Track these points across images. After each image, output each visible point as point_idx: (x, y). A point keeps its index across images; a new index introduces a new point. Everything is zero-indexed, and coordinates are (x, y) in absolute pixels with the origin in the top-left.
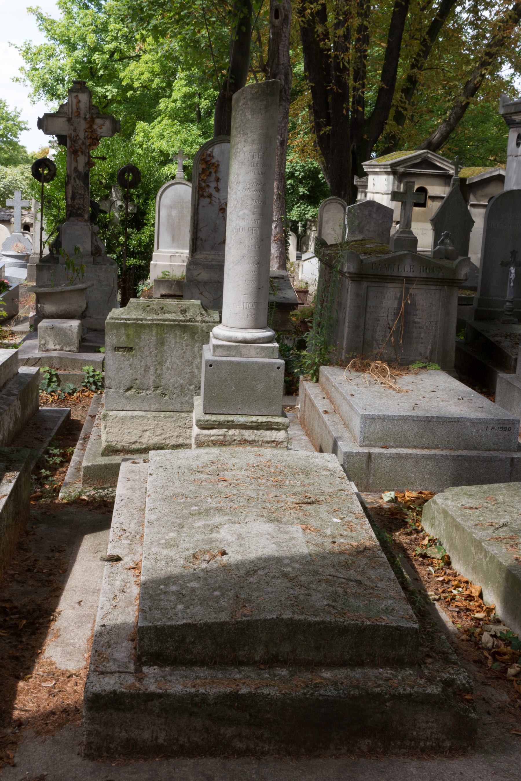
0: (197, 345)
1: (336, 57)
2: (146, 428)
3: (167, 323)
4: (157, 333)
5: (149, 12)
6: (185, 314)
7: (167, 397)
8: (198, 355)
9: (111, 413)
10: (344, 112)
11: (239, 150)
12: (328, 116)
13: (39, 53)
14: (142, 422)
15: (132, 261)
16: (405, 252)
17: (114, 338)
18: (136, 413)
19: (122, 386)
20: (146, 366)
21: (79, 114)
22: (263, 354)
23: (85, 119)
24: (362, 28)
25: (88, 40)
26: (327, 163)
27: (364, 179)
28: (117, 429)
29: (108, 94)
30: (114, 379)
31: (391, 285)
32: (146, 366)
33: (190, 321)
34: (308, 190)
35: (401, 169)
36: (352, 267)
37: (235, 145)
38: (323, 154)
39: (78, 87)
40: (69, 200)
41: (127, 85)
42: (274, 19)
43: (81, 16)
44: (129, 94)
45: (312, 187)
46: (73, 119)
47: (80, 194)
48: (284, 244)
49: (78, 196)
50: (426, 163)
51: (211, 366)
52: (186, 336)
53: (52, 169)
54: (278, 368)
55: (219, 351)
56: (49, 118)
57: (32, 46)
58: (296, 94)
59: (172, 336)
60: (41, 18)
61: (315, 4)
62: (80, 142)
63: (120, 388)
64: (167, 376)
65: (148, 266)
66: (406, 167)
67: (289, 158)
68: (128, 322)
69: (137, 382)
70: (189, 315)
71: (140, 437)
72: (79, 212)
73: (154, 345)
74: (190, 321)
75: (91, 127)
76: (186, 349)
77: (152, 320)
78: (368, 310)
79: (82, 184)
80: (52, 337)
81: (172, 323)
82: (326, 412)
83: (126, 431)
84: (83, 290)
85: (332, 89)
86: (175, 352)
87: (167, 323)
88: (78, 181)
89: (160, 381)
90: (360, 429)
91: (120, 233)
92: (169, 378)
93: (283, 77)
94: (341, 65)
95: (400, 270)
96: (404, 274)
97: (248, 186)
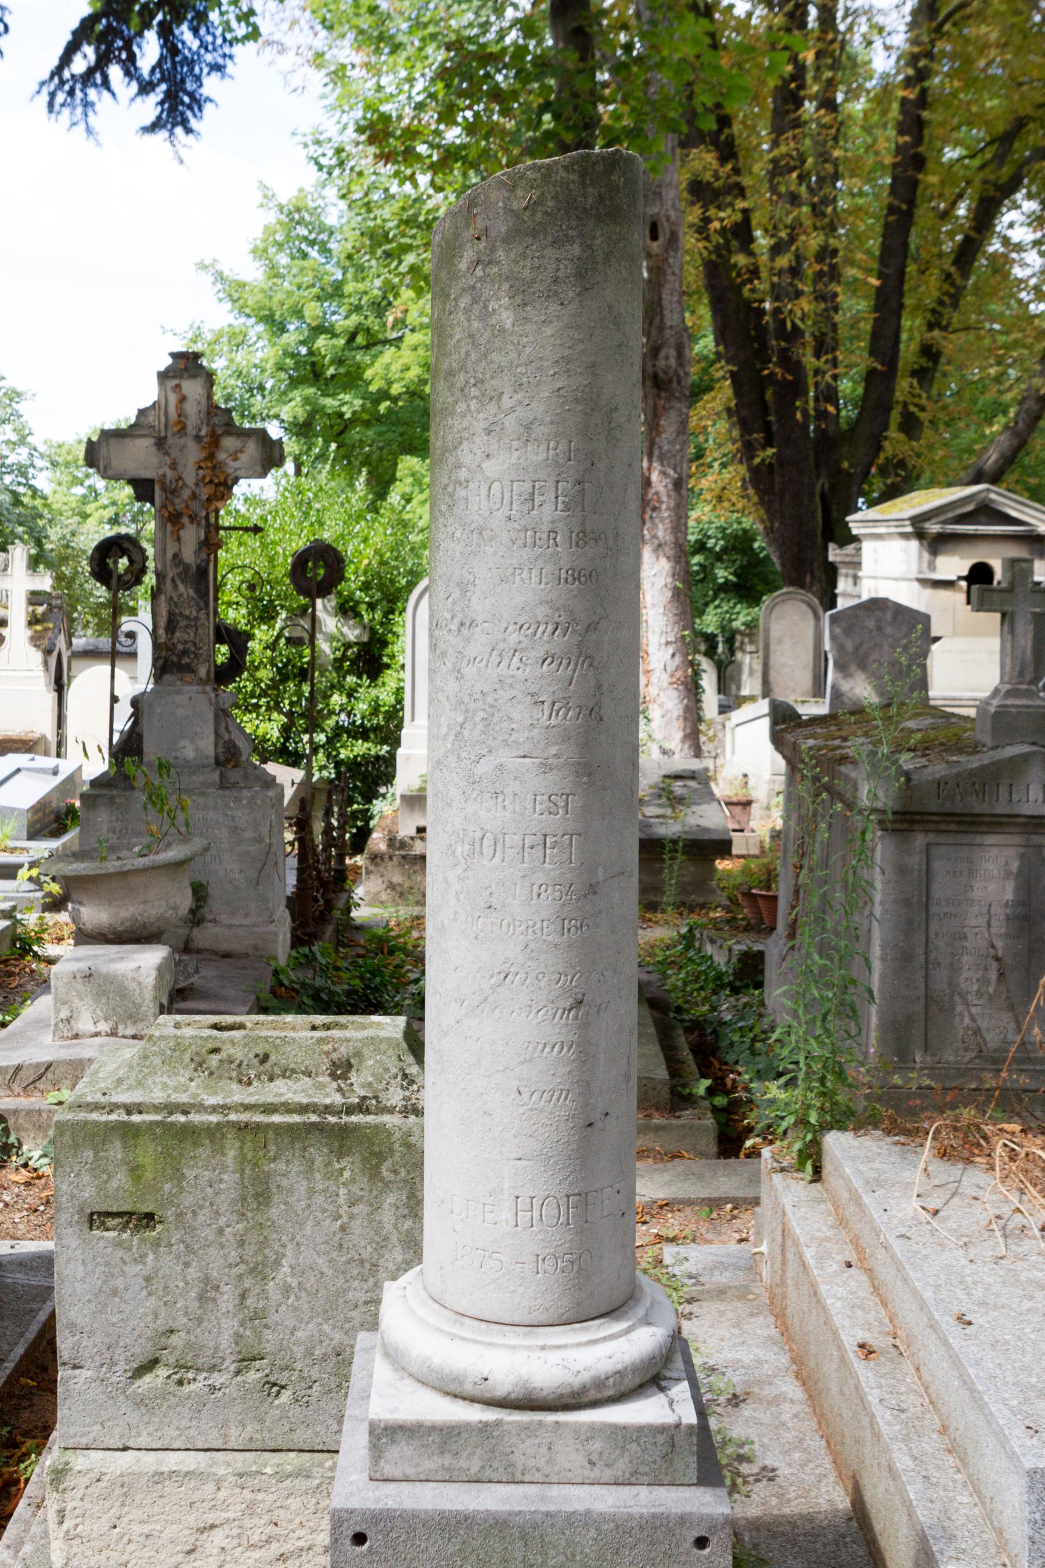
0: (390, 1199)
1: (777, 311)
2: (210, 1518)
3: (276, 1118)
4: (242, 1159)
5: (403, 240)
6: (345, 1077)
7: (286, 1396)
8: (394, 1238)
9: (80, 1461)
10: (799, 416)
11: (463, 474)
12: (767, 427)
13: (216, 342)
14: (196, 1496)
15: (360, 748)
16: (1025, 749)
17: (86, 1179)
18: (172, 1461)
19: (120, 1355)
20: (206, 1280)
21: (182, 429)
22: (622, 1466)
23: (198, 438)
24: (825, 253)
25: (307, 313)
26: (771, 521)
27: (850, 548)
28: (107, 1519)
29: (344, 409)
30: (92, 1333)
31: (991, 839)
32: (206, 1280)
33: (361, 1108)
34: (735, 574)
35: (933, 528)
36: (881, 794)
37: (445, 450)
38: (762, 502)
39: (182, 364)
40: (161, 631)
41: (379, 391)
42: (648, 241)
43: (294, 271)
44: (383, 407)
45: (741, 567)
46: (170, 441)
47: (188, 618)
48: (692, 689)
49: (183, 623)
50: (987, 512)
51: (360, 1539)
52: (349, 1167)
53: (137, 558)
54: (701, 1542)
55: (399, 1457)
56: (113, 441)
57: (205, 329)
58: (697, 392)
59: (296, 1167)
60: (220, 277)
61: (729, 211)
62: (186, 494)
63: (113, 1363)
64: (282, 1317)
65: (390, 761)
66: (944, 522)
67: (694, 514)
68: (136, 1118)
69: (175, 1340)
70: (359, 1082)
71: (189, 1552)
72: (186, 660)
73: (233, 1202)
74: (361, 1108)
75: (211, 456)
76: (351, 1217)
77: (224, 1109)
78: (934, 909)
79: (191, 592)
80: (89, 1001)
81: (296, 1118)
82: (866, 1350)
83: (137, 1529)
84: (178, 865)
85: (772, 374)
86: (308, 1229)
87: (276, 1118)
88: (181, 588)
89: (259, 1337)
90: (1027, 1530)
91: (332, 687)
92: (290, 1323)
93: (673, 353)
94: (789, 325)
95: (1015, 797)
96: (1028, 809)
97: (514, 638)
